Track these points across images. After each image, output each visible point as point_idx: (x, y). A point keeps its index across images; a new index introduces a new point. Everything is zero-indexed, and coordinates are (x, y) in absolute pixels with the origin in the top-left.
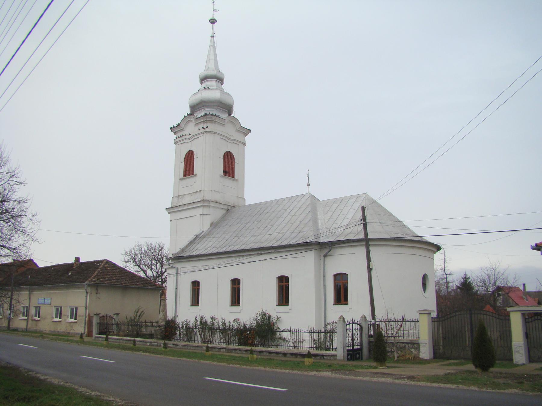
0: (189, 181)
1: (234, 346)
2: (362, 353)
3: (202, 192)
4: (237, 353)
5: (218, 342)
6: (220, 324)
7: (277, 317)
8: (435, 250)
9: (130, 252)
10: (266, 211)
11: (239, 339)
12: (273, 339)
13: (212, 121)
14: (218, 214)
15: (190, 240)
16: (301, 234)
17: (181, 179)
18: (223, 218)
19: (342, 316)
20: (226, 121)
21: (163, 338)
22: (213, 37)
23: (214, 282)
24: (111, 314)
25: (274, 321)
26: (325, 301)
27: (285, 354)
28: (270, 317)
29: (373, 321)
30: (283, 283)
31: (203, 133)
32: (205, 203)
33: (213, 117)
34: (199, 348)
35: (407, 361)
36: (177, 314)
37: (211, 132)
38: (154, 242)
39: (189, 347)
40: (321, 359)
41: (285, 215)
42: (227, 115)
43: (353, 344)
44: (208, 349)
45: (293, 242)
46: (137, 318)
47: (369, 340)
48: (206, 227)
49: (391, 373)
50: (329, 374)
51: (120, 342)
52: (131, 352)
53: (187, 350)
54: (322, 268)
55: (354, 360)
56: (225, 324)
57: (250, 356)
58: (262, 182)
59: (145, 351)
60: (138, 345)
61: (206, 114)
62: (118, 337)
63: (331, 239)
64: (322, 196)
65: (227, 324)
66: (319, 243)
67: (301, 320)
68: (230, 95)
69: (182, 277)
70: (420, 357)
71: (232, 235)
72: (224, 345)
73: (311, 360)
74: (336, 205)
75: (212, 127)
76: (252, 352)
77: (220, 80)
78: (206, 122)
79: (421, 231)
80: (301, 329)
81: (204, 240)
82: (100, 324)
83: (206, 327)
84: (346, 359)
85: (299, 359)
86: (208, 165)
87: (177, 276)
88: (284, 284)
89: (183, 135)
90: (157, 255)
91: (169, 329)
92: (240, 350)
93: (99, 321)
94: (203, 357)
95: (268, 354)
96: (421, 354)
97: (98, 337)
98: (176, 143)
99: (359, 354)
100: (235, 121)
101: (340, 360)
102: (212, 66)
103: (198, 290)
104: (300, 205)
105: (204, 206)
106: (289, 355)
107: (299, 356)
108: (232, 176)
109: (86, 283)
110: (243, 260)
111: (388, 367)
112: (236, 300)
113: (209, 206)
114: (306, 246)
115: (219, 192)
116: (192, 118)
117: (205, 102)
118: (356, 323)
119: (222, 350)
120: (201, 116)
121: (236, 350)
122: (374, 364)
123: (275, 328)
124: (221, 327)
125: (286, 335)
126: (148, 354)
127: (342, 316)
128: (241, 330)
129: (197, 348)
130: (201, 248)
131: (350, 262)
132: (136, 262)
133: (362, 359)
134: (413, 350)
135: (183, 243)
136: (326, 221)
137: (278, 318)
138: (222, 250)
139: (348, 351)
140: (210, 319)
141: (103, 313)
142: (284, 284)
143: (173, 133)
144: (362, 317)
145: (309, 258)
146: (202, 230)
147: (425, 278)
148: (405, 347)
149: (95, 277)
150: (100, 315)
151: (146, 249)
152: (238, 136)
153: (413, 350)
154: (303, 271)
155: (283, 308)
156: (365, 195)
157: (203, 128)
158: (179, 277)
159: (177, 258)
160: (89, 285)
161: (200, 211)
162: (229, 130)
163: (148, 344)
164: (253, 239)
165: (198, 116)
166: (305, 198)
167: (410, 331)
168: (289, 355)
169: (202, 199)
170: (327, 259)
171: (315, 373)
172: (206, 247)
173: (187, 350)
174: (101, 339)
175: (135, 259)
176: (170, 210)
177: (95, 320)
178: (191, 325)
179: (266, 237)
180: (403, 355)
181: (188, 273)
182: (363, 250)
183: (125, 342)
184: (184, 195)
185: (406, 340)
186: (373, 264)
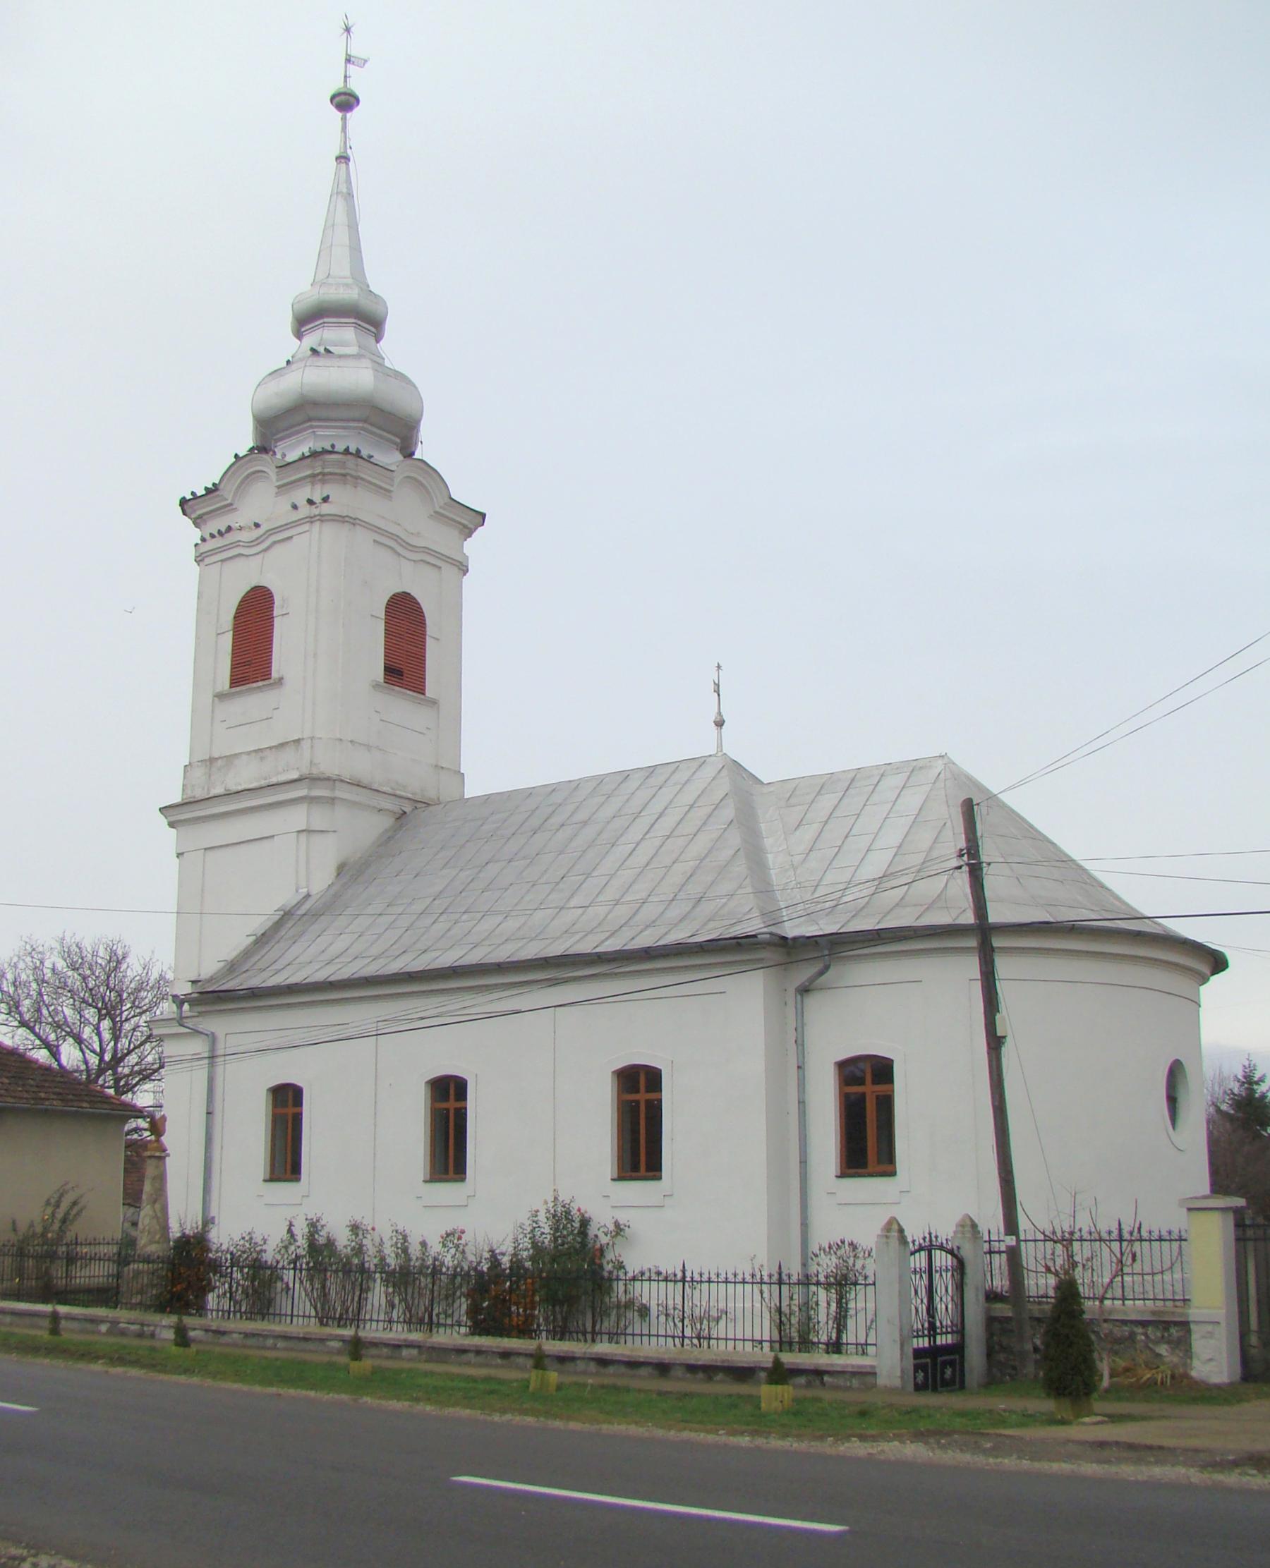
0: (254, 702)
1: (442, 1337)
2: (962, 1357)
3: (306, 745)
4: (468, 1364)
5: (381, 1319)
6: (388, 1251)
7: (617, 1224)
8: (1205, 969)
11: (473, 1311)
12: (600, 1312)
15: (258, 924)
16: (707, 908)
17: (220, 696)
18: (386, 845)
19: (893, 1221)
21: (162, 1307)
22: (343, 159)
23: (366, 1090)
25: (604, 1240)
26: (804, 1162)
27: (663, 1368)
28: (585, 1222)
29: (1011, 1241)
30: (639, 1094)
31: (311, 520)
32: (317, 788)
33: (351, 461)
34: (310, 1346)
35: (1148, 1391)
36: (213, 1212)
37: (340, 519)
38: (92, 934)
39: (270, 1342)
40: (809, 1385)
41: (636, 833)
42: (400, 457)
43: (932, 1327)
44: (356, 1347)
45: (679, 935)
46: (56, 1226)
47: (988, 1311)
48: (321, 880)
49: (1156, 1442)
50: (912, 1451)
52: (59, 1363)
53: (269, 1354)
54: (792, 1036)
55: (935, 1389)
56: (405, 1250)
57: (534, 1376)
58: (526, 713)
59: (119, 1358)
60: (70, 1334)
63: (828, 926)
64: (769, 767)
65: (415, 1250)
66: (783, 943)
67: (710, 1237)
68: (409, 382)
69: (229, 1072)
70: (1193, 1373)
72: (399, 1333)
73: (786, 1392)
74: (827, 801)
75: (343, 498)
76: (539, 1360)
77: (371, 322)
79: (1151, 897)
80: (727, 1269)
81: (316, 927)
83: (329, 1264)
84: (911, 1387)
85: (724, 1387)
86: (325, 645)
88: (452, 1104)
89: (229, 529)
90: (105, 991)
91: (188, 1270)
92: (479, 1352)
94: (328, 1377)
95: (593, 1367)
96: (1196, 1363)
98: (199, 559)
99: (952, 1363)
100: (428, 480)
101: (890, 1390)
102: (342, 269)
103: (298, 1119)
106: (679, 1372)
107: (720, 1376)
108: (417, 685)
111: (1114, 1418)
113: (332, 801)
114: (732, 950)
115: (368, 747)
116: (266, 464)
117: (315, 404)
118: (941, 1248)
119: (405, 1352)
120: (303, 458)
121: (462, 1351)
122: (1047, 1405)
123: (609, 1267)
124: (392, 1262)
125: (649, 1293)
126: (134, 1372)
127: (893, 1221)
128: (480, 1274)
129: (304, 1345)
130: (305, 960)
131: (914, 1019)
132: (21, 1014)
133: (962, 1386)
134: (1163, 1350)
136: (797, 859)
137: (619, 1229)
138: (395, 967)
139: (918, 1353)
142: (642, 1096)
143: (187, 522)
144: (961, 1225)
145: (746, 998)
147: (1175, 1073)
148: (1132, 1335)
151: (61, 965)
152: (438, 537)
153: (1163, 1350)
154: (717, 1047)
155: (637, 1190)
156: (940, 765)
157: (310, 502)
158: (219, 1070)
159: (213, 998)
161: (297, 817)
162: (407, 513)
163: (104, 1328)
164: (511, 924)
165: (289, 459)
166: (708, 772)
167: (1167, 1277)
168: (679, 1372)
169: (305, 771)
170: (812, 1001)
171: (857, 1448)
173: (269, 1354)
176: (178, 814)
178: (269, 1257)
179: (568, 917)
180: (1127, 1370)
181: (259, 1055)
182: (971, 967)
184: (230, 759)
185: (1135, 1309)
186: (1007, 1021)
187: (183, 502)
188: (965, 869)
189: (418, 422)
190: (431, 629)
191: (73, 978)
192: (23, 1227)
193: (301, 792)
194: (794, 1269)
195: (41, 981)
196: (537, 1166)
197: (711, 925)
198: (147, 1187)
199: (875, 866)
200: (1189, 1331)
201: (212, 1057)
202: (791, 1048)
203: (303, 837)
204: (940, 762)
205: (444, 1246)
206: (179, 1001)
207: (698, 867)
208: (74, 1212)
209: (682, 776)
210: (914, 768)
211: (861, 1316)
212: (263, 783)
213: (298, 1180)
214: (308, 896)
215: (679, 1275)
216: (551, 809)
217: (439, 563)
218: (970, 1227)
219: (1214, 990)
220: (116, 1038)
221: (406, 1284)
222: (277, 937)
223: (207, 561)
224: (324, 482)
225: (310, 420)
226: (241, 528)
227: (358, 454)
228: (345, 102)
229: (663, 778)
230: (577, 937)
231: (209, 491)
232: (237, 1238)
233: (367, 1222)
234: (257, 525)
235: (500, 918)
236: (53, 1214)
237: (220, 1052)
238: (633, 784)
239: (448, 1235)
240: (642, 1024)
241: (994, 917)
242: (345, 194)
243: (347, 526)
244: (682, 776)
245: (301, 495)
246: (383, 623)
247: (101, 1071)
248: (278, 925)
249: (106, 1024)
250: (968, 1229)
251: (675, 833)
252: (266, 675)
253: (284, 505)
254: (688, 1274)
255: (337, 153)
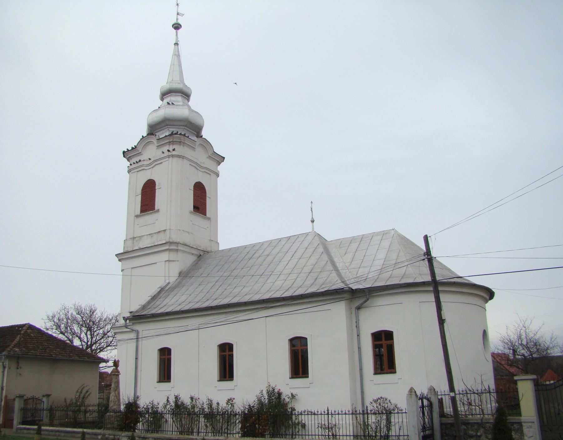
0: (149, 218)
3: (168, 232)
6: (205, 406)
7: (292, 394)
9: (54, 317)
10: (257, 255)
13: (180, 143)
14: (187, 260)
16: (320, 281)
17: (137, 216)
20: (197, 144)
22: (176, 44)
24: (39, 395)
25: (287, 400)
26: (361, 369)
28: (280, 394)
29: (452, 394)
31: (169, 157)
32: (172, 246)
36: (138, 394)
37: (179, 156)
38: (85, 303)
46: (80, 400)
47: (440, 420)
51: (59, 436)
54: (354, 325)
56: (211, 406)
58: (242, 220)
61: (172, 134)
62: (51, 428)
64: (329, 237)
65: (215, 405)
68: (199, 114)
69: (143, 344)
71: (201, 288)
74: (354, 246)
75: (179, 150)
77: (186, 95)
78: (173, 143)
82: (24, 410)
86: (173, 199)
87: (137, 342)
89: (140, 161)
90: (89, 322)
93: (22, 406)
97: (21, 429)
98: (129, 172)
100: (206, 145)
104: (305, 244)
105: (170, 250)
109: (4, 353)
110: (242, 316)
112: (226, 371)
115: (188, 232)
116: (153, 139)
120: (166, 136)
124: (206, 410)
125: (304, 419)
135: (143, 299)
136: (347, 264)
137: (293, 396)
140: (190, 400)
141: (29, 395)
142: (227, 353)
143: (125, 159)
145: (339, 311)
146: (168, 281)
149: (16, 346)
150: (25, 398)
151: (75, 313)
152: (210, 164)
157: (169, 151)
158: (140, 343)
159: (137, 318)
160: (7, 357)
161: (165, 256)
162: (200, 156)
166: (310, 238)
169: (167, 240)
172: (178, 302)
174: (25, 431)
175: (60, 327)
176: (121, 257)
177: (18, 405)
181: (154, 338)
183: (63, 434)
184: (141, 237)
186: (446, 314)
187: (124, 152)
188: (426, 260)
189: (202, 127)
190: (208, 194)
191: (79, 318)
192: (68, 401)
193: (167, 247)
194: (359, 409)
195: (68, 319)
196: (260, 374)
197: (323, 286)
198: (113, 386)
199: (378, 264)
200: (521, 426)
201: (137, 339)
202: (355, 328)
203: (167, 262)
204: (393, 231)
205: (227, 404)
206: (125, 319)
207: (313, 268)
208: (87, 394)
209: (301, 239)
210: (384, 234)
211: (397, 426)
212: (153, 245)
213: (170, 382)
214: (169, 283)
215: (326, 412)
216: (254, 252)
217: (210, 173)
218: (432, 390)
219: (490, 305)
220: (92, 338)
221: (212, 418)
222: (159, 297)
223: (132, 172)
224: (173, 144)
225: (167, 125)
226: (144, 160)
227: (184, 135)
228: (177, 27)
229: (294, 240)
230: (273, 292)
231: (133, 148)
232: (148, 403)
233: (196, 396)
234: (150, 159)
235: (242, 287)
236: (79, 396)
237: (140, 336)
238: (283, 243)
239: (229, 400)
240: (298, 322)
241: (438, 278)
242: (177, 55)
243: (181, 159)
244: (301, 239)
245: (165, 149)
246: (192, 192)
247: (87, 348)
248: (159, 293)
249: (89, 333)
250: (432, 391)
251: (303, 257)
252: (154, 209)
253: (159, 152)
254: (330, 412)
255: (175, 42)
